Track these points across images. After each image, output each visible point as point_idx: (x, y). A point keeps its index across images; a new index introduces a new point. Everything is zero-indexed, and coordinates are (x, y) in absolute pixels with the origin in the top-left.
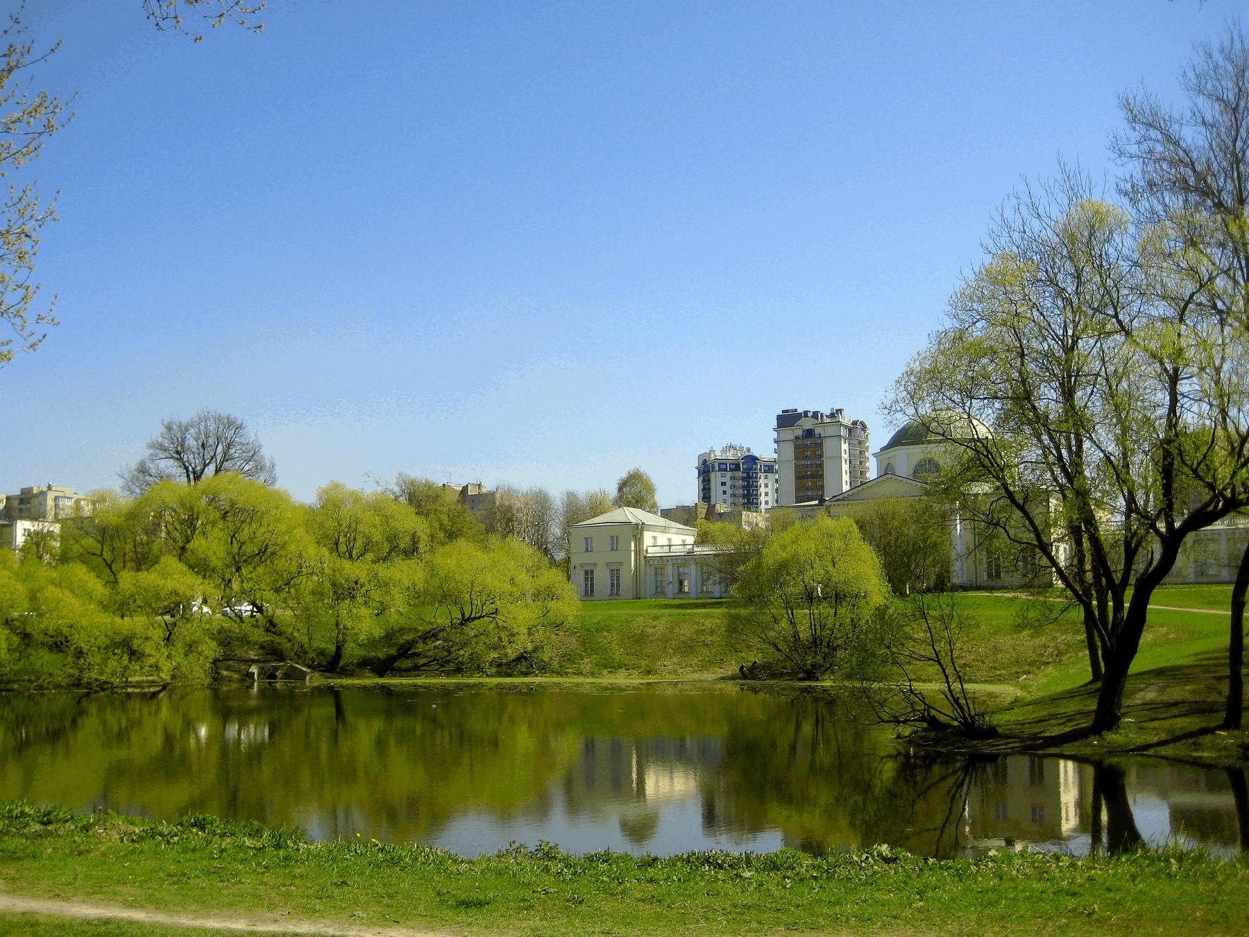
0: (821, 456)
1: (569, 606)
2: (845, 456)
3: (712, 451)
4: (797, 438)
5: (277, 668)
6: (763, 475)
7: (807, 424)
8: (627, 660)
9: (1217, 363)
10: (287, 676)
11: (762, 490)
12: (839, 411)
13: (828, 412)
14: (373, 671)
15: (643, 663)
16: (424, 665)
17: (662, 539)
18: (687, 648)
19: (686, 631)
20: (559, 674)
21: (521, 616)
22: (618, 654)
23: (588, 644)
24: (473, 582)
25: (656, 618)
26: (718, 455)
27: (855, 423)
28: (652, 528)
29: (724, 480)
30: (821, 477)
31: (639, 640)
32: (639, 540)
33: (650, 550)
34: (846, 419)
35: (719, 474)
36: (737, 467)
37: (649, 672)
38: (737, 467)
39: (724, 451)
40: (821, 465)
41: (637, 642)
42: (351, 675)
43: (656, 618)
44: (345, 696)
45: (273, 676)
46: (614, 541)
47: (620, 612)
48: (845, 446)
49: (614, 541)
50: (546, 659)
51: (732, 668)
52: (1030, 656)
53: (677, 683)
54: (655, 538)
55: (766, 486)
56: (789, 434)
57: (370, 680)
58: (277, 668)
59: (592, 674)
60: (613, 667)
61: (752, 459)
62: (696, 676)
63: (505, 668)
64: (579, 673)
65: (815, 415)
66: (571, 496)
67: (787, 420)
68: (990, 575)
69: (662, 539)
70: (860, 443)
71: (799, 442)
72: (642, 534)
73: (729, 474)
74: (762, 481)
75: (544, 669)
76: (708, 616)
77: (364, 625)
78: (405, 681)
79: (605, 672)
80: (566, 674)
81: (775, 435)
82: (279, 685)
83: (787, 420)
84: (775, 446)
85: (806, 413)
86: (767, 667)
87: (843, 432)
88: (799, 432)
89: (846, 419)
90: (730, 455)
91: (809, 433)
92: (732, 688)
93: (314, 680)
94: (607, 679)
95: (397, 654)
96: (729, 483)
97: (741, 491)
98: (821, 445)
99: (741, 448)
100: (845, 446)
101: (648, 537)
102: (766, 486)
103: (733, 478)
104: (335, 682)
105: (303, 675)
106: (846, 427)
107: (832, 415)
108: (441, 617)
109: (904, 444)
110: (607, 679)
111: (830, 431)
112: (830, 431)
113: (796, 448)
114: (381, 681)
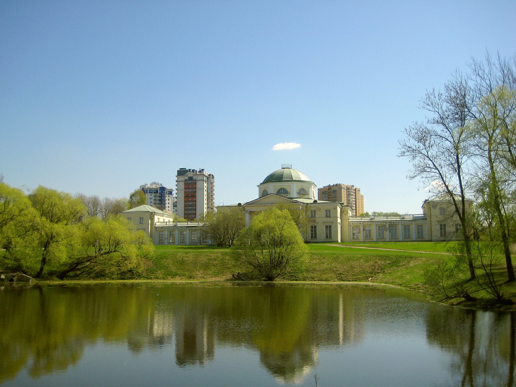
0: (196, 188)
1: (150, 248)
2: (205, 189)
3: (146, 184)
4: (186, 180)
5: (14, 276)
6: (167, 195)
7: (190, 174)
8: (179, 272)
9: (426, 154)
10: (19, 280)
11: (167, 202)
12: (203, 170)
13: (198, 170)
14: (58, 277)
15: (187, 273)
16: (80, 274)
17: (161, 219)
18: (206, 267)
19: (203, 259)
20: (147, 278)
21: (133, 251)
22: (173, 269)
23: (156, 265)
24: (227, 225)
25: (186, 253)
26: (149, 186)
27: (210, 175)
28: (158, 214)
29: (151, 197)
30: (195, 197)
31: (182, 263)
32: (152, 219)
33: (157, 224)
34: (206, 173)
35: (149, 194)
36: (157, 192)
37: (190, 278)
38: (157, 192)
39: (151, 184)
40: (195, 192)
41: (181, 264)
42: (47, 279)
43: (186, 253)
44: (44, 290)
45: (12, 280)
46: (141, 219)
47: (169, 250)
48: (205, 185)
49: (141, 219)
50: (140, 271)
51: (229, 276)
52: (369, 270)
53: (204, 282)
54: (158, 218)
55: (169, 200)
56: (182, 178)
57: (58, 282)
58: (14, 276)
59: (164, 279)
60: (174, 275)
61: (163, 189)
62: (214, 279)
63: (123, 275)
64: (157, 278)
65: (193, 171)
66: (107, 199)
67: (182, 172)
68: (312, 237)
69: (161, 219)
70: (211, 183)
71: (186, 182)
72: (154, 217)
73: (153, 194)
74: (167, 198)
75: (139, 276)
76: (211, 253)
77: (61, 254)
78: (73, 282)
79: (169, 277)
80: (151, 278)
81: (176, 179)
82: (15, 284)
83: (182, 172)
84: (176, 183)
85: (190, 170)
86: (245, 275)
87: (205, 178)
88: (187, 178)
89: (206, 173)
90: (154, 186)
91: (191, 178)
92: (229, 284)
93: (33, 282)
94: (170, 281)
95: (73, 268)
96: (153, 198)
97: (158, 202)
98: (196, 183)
99: (158, 184)
100: (205, 185)
101: (156, 218)
102: (169, 200)
103: (155, 196)
104: (42, 283)
105: (28, 280)
106: (206, 176)
107: (200, 172)
108: (92, 251)
109: (273, 182)
110: (170, 281)
111: (200, 178)
112: (200, 178)
113: (185, 184)
114: (61, 282)
